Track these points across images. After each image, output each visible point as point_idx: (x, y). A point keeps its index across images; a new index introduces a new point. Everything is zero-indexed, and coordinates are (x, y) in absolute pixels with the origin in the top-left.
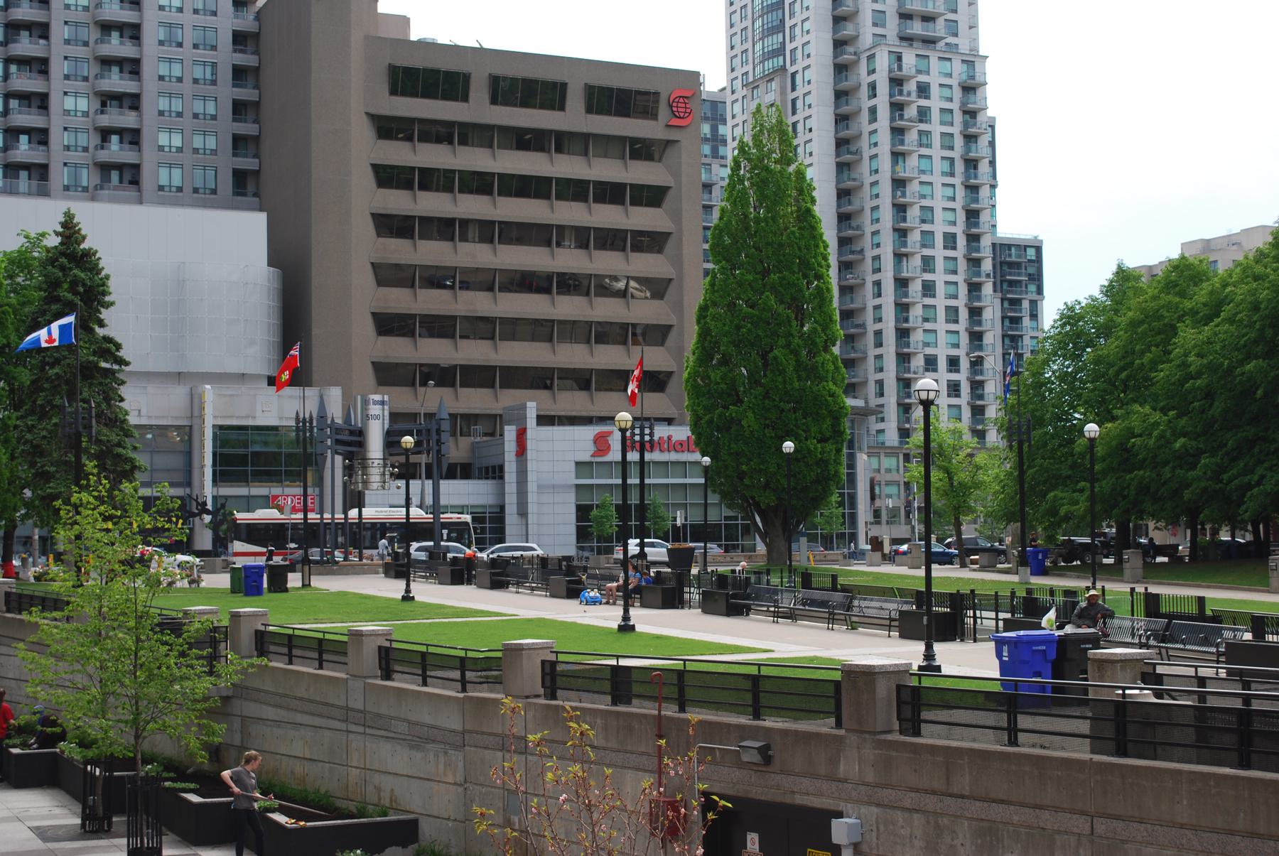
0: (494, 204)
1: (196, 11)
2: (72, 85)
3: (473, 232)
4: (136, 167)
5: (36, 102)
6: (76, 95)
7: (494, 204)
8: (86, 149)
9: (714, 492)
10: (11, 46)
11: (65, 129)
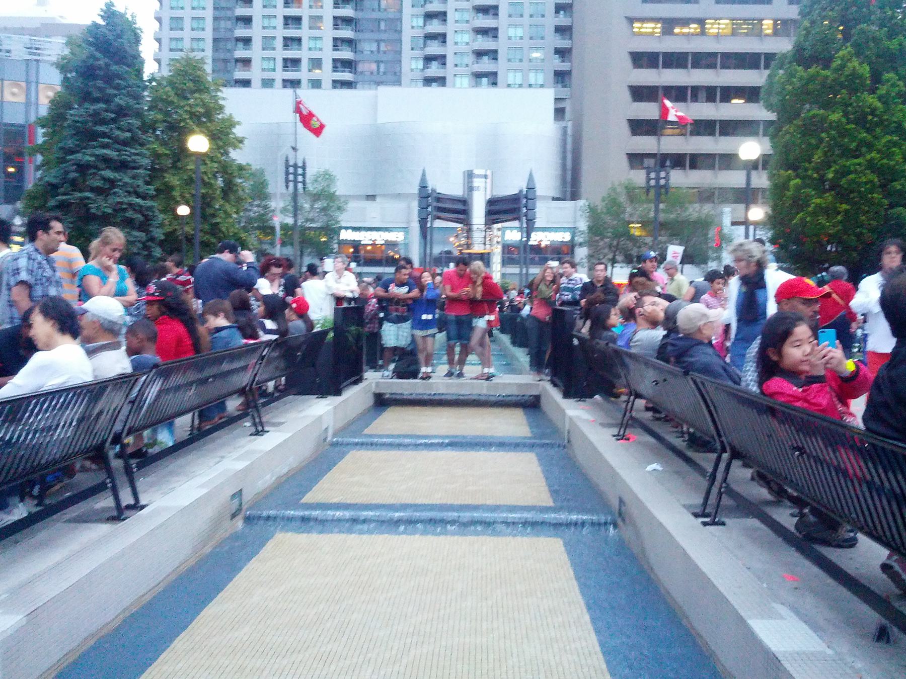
3: (702, 95)
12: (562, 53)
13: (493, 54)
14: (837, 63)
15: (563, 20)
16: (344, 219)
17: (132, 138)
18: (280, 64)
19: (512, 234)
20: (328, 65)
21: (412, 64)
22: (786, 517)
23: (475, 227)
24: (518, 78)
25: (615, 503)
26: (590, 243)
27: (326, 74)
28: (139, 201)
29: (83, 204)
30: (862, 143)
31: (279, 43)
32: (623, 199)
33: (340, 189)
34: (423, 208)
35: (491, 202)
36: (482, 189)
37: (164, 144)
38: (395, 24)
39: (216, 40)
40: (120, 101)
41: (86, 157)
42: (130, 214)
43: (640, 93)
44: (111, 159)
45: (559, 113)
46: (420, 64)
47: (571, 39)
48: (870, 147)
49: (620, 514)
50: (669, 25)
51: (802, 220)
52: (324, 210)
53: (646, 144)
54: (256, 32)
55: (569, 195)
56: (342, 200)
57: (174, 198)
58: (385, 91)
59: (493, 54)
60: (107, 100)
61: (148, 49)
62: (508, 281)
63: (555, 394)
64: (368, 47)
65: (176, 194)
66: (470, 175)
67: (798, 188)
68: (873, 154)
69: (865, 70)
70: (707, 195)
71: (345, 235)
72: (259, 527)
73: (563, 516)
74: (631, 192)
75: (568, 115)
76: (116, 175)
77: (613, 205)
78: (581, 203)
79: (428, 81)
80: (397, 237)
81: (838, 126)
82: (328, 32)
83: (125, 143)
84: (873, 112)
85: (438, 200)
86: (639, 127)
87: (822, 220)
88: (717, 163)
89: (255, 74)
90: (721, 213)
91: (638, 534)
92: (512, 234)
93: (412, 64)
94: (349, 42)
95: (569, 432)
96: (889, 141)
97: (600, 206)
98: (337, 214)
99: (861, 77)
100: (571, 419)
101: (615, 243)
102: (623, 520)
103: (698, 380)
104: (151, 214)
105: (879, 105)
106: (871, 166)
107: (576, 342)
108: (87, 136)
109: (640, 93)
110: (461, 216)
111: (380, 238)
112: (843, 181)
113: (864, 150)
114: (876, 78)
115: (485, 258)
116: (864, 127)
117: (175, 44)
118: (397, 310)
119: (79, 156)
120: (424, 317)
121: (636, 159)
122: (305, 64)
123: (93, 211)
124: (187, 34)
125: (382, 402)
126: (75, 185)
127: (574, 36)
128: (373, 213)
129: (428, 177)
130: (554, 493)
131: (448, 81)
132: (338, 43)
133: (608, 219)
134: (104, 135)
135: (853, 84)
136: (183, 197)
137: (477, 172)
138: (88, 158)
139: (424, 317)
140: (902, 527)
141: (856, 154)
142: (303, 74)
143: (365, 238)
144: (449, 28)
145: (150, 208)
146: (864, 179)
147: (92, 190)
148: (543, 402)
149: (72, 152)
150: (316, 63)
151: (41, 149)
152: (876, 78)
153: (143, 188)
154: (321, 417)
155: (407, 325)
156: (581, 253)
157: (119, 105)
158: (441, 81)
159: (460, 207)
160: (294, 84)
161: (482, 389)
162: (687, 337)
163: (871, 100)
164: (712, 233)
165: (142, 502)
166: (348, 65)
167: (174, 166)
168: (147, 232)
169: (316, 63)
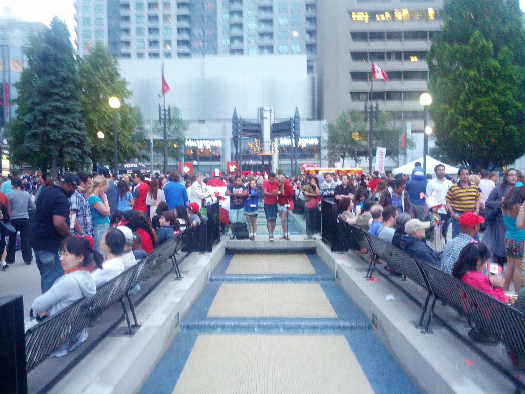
3: (394, 56)
12: (311, 33)
13: (270, 35)
14: (472, 41)
15: (311, 13)
16: (187, 134)
17: (72, 96)
18: (147, 43)
19: (286, 141)
20: (174, 43)
21: (223, 41)
22: (464, 330)
23: (265, 141)
24: (286, 48)
25: (370, 317)
26: (329, 147)
27: (174, 48)
28: (78, 132)
29: (46, 134)
30: (489, 88)
31: (146, 31)
32: (349, 120)
33: (184, 116)
34: (235, 130)
35: (274, 126)
36: (269, 119)
37: (87, 96)
38: (213, 18)
39: (109, 31)
40: (64, 74)
41: (46, 107)
42: (72, 139)
43: (357, 56)
44: (60, 108)
45: (310, 68)
46: (228, 41)
47: (316, 25)
48: (493, 90)
49: (373, 321)
50: (372, 15)
51: (455, 134)
52: (176, 129)
53: (362, 86)
54: (133, 25)
55: (316, 117)
56: (186, 123)
57: (94, 128)
58: (209, 59)
59: (270, 35)
60: (56, 74)
61: (73, 38)
62: (282, 169)
63: (326, 249)
64: (197, 32)
65: (96, 125)
66: (261, 110)
67: (452, 114)
68: (496, 95)
69: (491, 45)
70: (397, 115)
71: (189, 143)
72: (192, 332)
73: (342, 323)
74: (353, 114)
75: (315, 69)
76: (64, 117)
77: (343, 123)
78: (324, 122)
79: (233, 52)
80: (218, 144)
81: (476, 79)
82: (174, 23)
83: (67, 99)
84: (495, 69)
85: (244, 125)
86: (357, 76)
87: (466, 133)
88: (403, 95)
89: (133, 50)
90: (405, 128)
91: (384, 333)
92: (286, 141)
93: (223, 41)
94: (188, 30)
95: (337, 272)
96: (505, 87)
97: (335, 124)
98: (184, 132)
99: (488, 50)
100: (338, 265)
101: (345, 146)
102: (376, 326)
103: (419, 262)
104: (83, 138)
105: (499, 65)
106: (495, 101)
107: (338, 221)
108: (46, 95)
109: (357, 56)
110: (258, 134)
111: (209, 145)
112: (478, 111)
113: (490, 92)
114: (496, 48)
115: (269, 158)
116: (490, 78)
117: (86, 34)
118: (238, 202)
119: (42, 107)
120: (252, 206)
121: (355, 95)
122: (161, 43)
123: (52, 138)
124: (92, 27)
125: (230, 252)
126: (41, 123)
127: (318, 24)
128: (204, 130)
129: (238, 112)
130: (337, 310)
131: (245, 51)
132: (180, 30)
133: (340, 132)
134: (56, 94)
135: (483, 53)
136: (99, 126)
137: (265, 108)
138: (47, 108)
139: (252, 206)
140: (523, 337)
141: (485, 94)
142: (161, 49)
143: (200, 145)
144: (245, 20)
145: (83, 136)
146: (490, 110)
147: (50, 126)
148: (318, 251)
149: (38, 104)
150: (168, 42)
151: (16, 101)
152: (496, 48)
153: (78, 124)
154: (206, 266)
155: (242, 210)
156: (325, 153)
157: (63, 77)
158: (241, 51)
159: (256, 128)
160: (155, 55)
161: (285, 245)
162: (410, 237)
163: (494, 63)
164: (401, 139)
165: (139, 324)
166: (186, 43)
167: (93, 108)
168: (82, 149)
169: (168, 42)
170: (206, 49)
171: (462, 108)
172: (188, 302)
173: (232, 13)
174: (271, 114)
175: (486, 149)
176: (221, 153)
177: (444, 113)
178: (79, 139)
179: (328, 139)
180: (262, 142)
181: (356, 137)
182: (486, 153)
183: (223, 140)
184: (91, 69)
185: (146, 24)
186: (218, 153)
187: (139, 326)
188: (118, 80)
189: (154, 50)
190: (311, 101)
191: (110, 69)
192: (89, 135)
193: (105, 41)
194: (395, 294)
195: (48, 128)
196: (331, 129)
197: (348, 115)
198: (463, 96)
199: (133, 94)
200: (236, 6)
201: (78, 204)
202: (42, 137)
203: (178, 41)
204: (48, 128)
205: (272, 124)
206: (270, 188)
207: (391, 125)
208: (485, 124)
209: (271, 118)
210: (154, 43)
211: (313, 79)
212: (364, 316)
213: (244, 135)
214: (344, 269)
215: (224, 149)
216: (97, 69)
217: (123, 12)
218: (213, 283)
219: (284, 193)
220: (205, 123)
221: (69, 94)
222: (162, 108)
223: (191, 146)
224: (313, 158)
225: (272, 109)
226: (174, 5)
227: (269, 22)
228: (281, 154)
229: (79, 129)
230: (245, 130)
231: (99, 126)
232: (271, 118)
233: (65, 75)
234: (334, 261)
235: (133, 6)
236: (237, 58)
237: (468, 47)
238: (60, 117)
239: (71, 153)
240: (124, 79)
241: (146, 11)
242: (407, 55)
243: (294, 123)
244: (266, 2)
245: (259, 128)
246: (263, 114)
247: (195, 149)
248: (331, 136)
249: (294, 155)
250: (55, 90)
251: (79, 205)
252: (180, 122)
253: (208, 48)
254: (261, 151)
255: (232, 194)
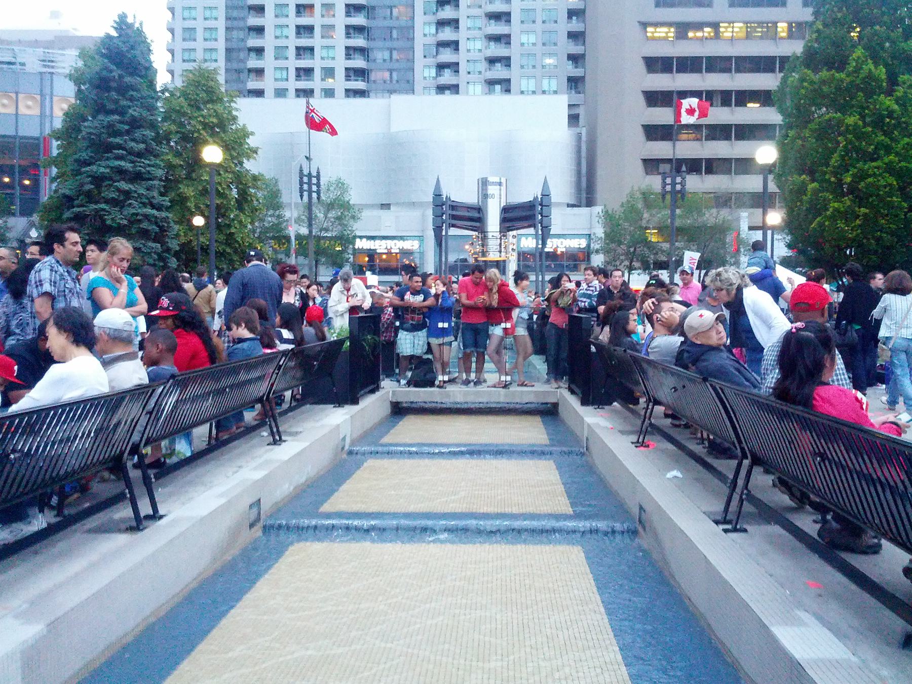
0: (702, 146)
1: (544, 44)
2: (472, 33)
3: (718, 99)
4: (509, 81)
5: (453, 46)
6: (474, 39)
7: (702, 146)
8: (480, 51)
9: (638, 260)
10: (439, 57)
11: (468, 17)
12: (575, 59)
13: (506, 61)
15: (575, 25)
16: (358, 228)
18: (292, 73)
20: (340, 73)
21: (424, 71)
23: (490, 235)
24: (532, 85)
27: (339, 83)
28: (154, 212)
31: (292, 52)
33: (354, 197)
34: (437, 216)
35: (505, 210)
36: (497, 196)
37: (178, 154)
38: (408, 32)
39: (228, 51)
41: (101, 169)
42: (145, 225)
45: (573, 119)
48: (888, 150)
50: (682, 29)
51: (821, 225)
54: (268, 41)
58: (398, 100)
59: (506, 61)
63: (573, 402)
64: (380, 55)
65: (191, 205)
66: (484, 183)
67: (815, 192)
69: (881, 72)
70: (724, 200)
71: (360, 244)
75: (533, 47)
76: (131, 186)
77: (631, 211)
78: (598, 209)
79: (441, 89)
80: (411, 245)
82: (340, 41)
83: (139, 155)
84: (891, 115)
87: (841, 224)
89: (268, 83)
90: (738, 219)
92: (528, 240)
93: (424, 71)
95: (587, 439)
98: (351, 222)
99: (877, 80)
100: (589, 425)
101: (632, 250)
102: (644, 528)
105: (896, 107)
106: (890, 169)
107: (593, 349)
108: (102, 148)
110: (477, 224)
111: (396, 246)
120: (440, 325)
121: (651, 165)
122: (317, 73)
123: (108, 222)
125: (399, 410)
126: (90, 197)
128: (388, 222)
132: (350, 51)
134: (120, 147)
135: (869, 87)
136: (197, 207)
137: (491, 179)
138: (102, 170)
139: (440, 325)
142: (316, 83)
143: (380, 246)
144: (462, 36)
145: (166, 219)
146: (883, 183)
147: (107, 202)
149: (87, 163)
150: (329, 72)
152: (893, 81)
153: (158, 199)
158: (454, 89)
159: (475, 215)
163: (889, 102)
164: (729, 238)
166: (361, 73)
167: (189, 177)
168: (163, 244)
169: (329, 72)
170: (394, 82)
171: (833, 179)
172: (287, 486)
173: (441, 24)
174: (500, 190)
175: (876, 252)
176: (417, 261)
177: (801, 190)
178: (156, 223)
179: (603, 235)
180: (484, 238)
181: (653, 237)
182: (874, 258)
183: (421, 238)
184: (185, 104)
185: (293, 42)
186: (413, 260)
187: (161, 517)
188: (234, 127)
189: (303, 84)
190: (573, 173)
191: (219, 107)
192: (179, 222)
193: (219, 65)
194: (684, 470)
195: (103, 206)
196: (609, 218)
197: (638, 195)
198: (835, 160)
199: (260, 152)
200: (447, 13)
201: (54, 283)
202: (91, 220)
203: (346, 68)
204: (103, 206)
205: (502, 206)
206: (473, 291)
207: (712, 216)
208: (871, 207)
209: (500, 195)
210: (305, 73)
211: (579, 137)
212: (620, 509)
213: (453, 226)
214: (597, 431)
215: (422, 254)
216: (199, 109)
217: (254, 21)
218: (353, 457)
219: (495, 303)
220: (389, 209)
221: (142, 146)
222: (306, 172)
223: (365, 248)
224: (577, 271)
225: (503, 180)
226: (340, 10)
227: (502, 39)
228: (522, 263)
229: (159, 208)
230: (454, 217)
231: (197, 207)
232: (500, 195)
233: (136, 114)
234: (583, 419)
235: (270, 11)
236: (448, 98)
237: (842, 75)
238: (124, 185)
239: (143, 249)
240: (244, 125)
241: (293, 20)
242: (743, 98)
243: (541, 205)
244: (499, 7)
245: (479, 213)
246: (486, 190)
247: (372, 254)
248: (608, 231)
249: (541, 266)
250: (118, 140)
251: (55, 286)
252: (346, 206)
253: (397, 81)
254: (484, 254)
255: (402, 303)
